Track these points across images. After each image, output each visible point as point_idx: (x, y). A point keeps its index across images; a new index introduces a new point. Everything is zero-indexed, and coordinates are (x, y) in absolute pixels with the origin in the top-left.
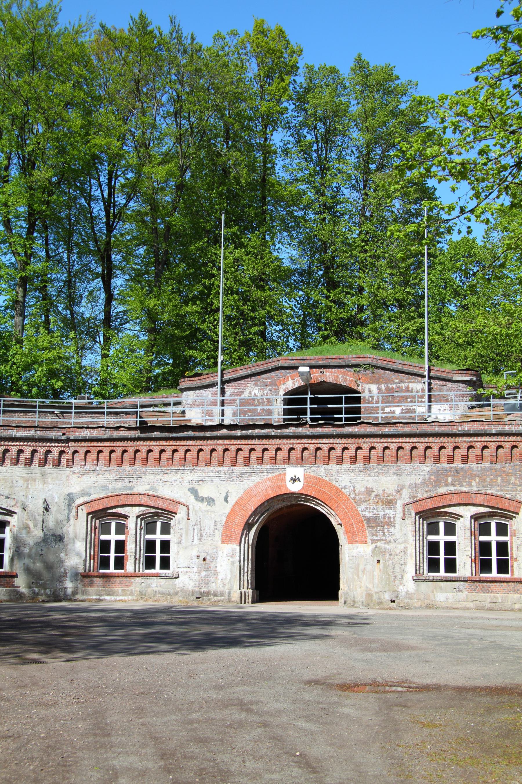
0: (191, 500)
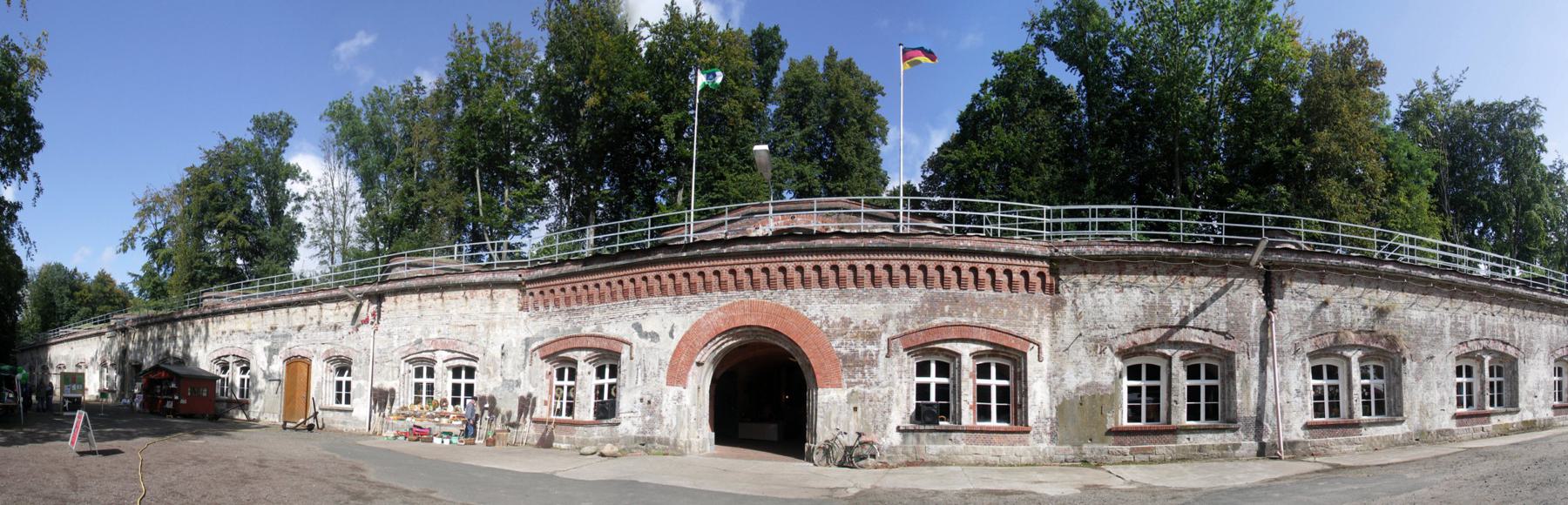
0: (634, 337)
